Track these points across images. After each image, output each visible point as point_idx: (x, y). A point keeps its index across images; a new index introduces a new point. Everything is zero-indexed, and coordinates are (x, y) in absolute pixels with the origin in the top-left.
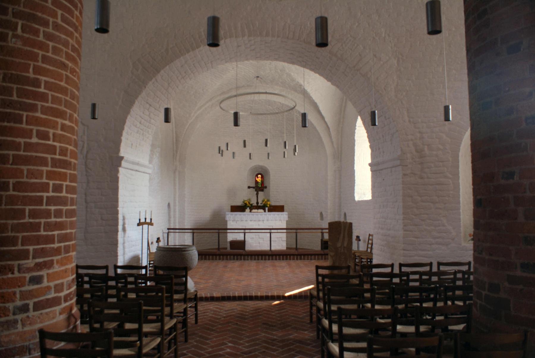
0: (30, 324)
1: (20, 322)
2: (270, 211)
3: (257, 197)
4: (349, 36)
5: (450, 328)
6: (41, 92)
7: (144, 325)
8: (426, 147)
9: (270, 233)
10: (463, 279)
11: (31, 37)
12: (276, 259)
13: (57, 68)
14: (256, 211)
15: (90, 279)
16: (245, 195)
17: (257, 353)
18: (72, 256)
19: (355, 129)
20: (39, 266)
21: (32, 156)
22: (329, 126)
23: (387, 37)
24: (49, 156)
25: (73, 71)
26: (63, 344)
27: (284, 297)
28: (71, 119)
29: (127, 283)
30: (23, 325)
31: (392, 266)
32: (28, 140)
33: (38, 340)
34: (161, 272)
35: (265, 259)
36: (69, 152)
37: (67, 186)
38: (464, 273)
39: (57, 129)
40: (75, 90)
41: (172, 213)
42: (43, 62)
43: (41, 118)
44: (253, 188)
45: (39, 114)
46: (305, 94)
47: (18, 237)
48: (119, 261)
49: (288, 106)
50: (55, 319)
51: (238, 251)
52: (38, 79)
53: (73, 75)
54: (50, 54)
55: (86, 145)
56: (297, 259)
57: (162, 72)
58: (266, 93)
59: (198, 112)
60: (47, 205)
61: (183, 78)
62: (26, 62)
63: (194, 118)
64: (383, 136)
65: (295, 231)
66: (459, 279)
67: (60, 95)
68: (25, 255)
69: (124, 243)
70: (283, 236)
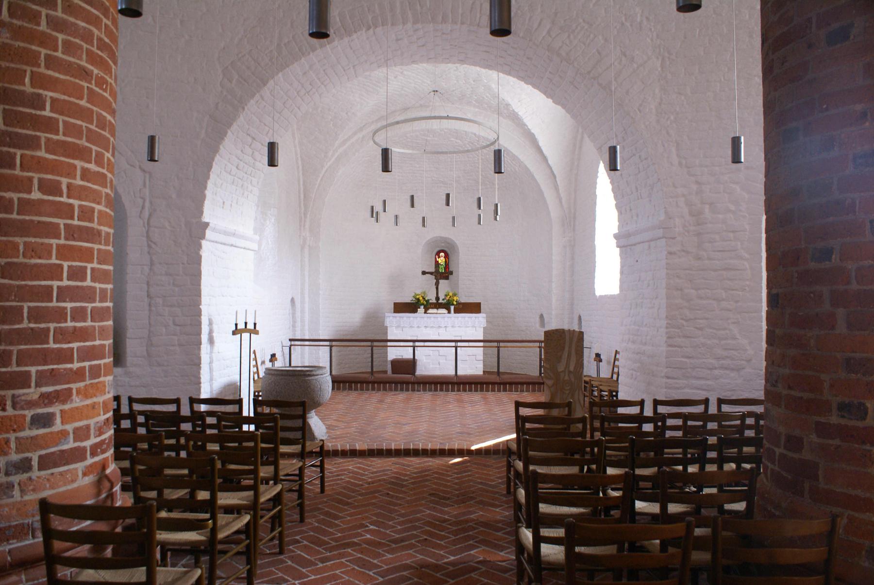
0: (34, 490)
1: (16, 486)
2: (457, 311)
3: (437, 288)
4: (581, 21)
5: (727, 507)
6: (45, 116)
7: (220, 494)
8: (707, 206)
9: (414, 347)
10: (756, 427)
11: (25, 24)
12: (465, 390)
13: (72, 76)
14: (435, 311)
15: (147, 419)
17: (413, 541)
18: (104, 382)
19: (597, 177)
20: (47, 399)
21: (32, 221)
23: (645, 22)
24: (61, 222)
25: (101, 82)
26: (89, 522)
27: (470, 452)
28: (99, 161)
29: (205, 426)
30: (23, 492)
31: (641, 403)
32: (25, 196)
33: (38, 518)
34: (267, 410)
35: (447, 390)
36: (96, 214)
37: (93, 269)
38: (757, 417)
39: (75, 178)
40: (105, 114)
41: (298, 314)
42: (47, 67)
43: (46, 159)
44: (431, 273)
45: (42, 153)
46: (515, 119)
47: (11, 352)
48: (202, 390)
49: (488, 140)
50: (76, 483)
51: (404, 377)
52: (39, 95)
53: (101, 88)
54: (59, 54)
55: (147, 204)
56: (499, 391)
57: (271, 83)
58: (448, 118)
59: (341, 150)
60: (58, 301)
61: (308, 92)
62: (18, 66)
63: (333, 159)
64: (637, 188)
65: (495, 344)
66: (750, 427)
67: (79, 122)
68: (23, 380)
69: (211, 363)
70: (478, 352)
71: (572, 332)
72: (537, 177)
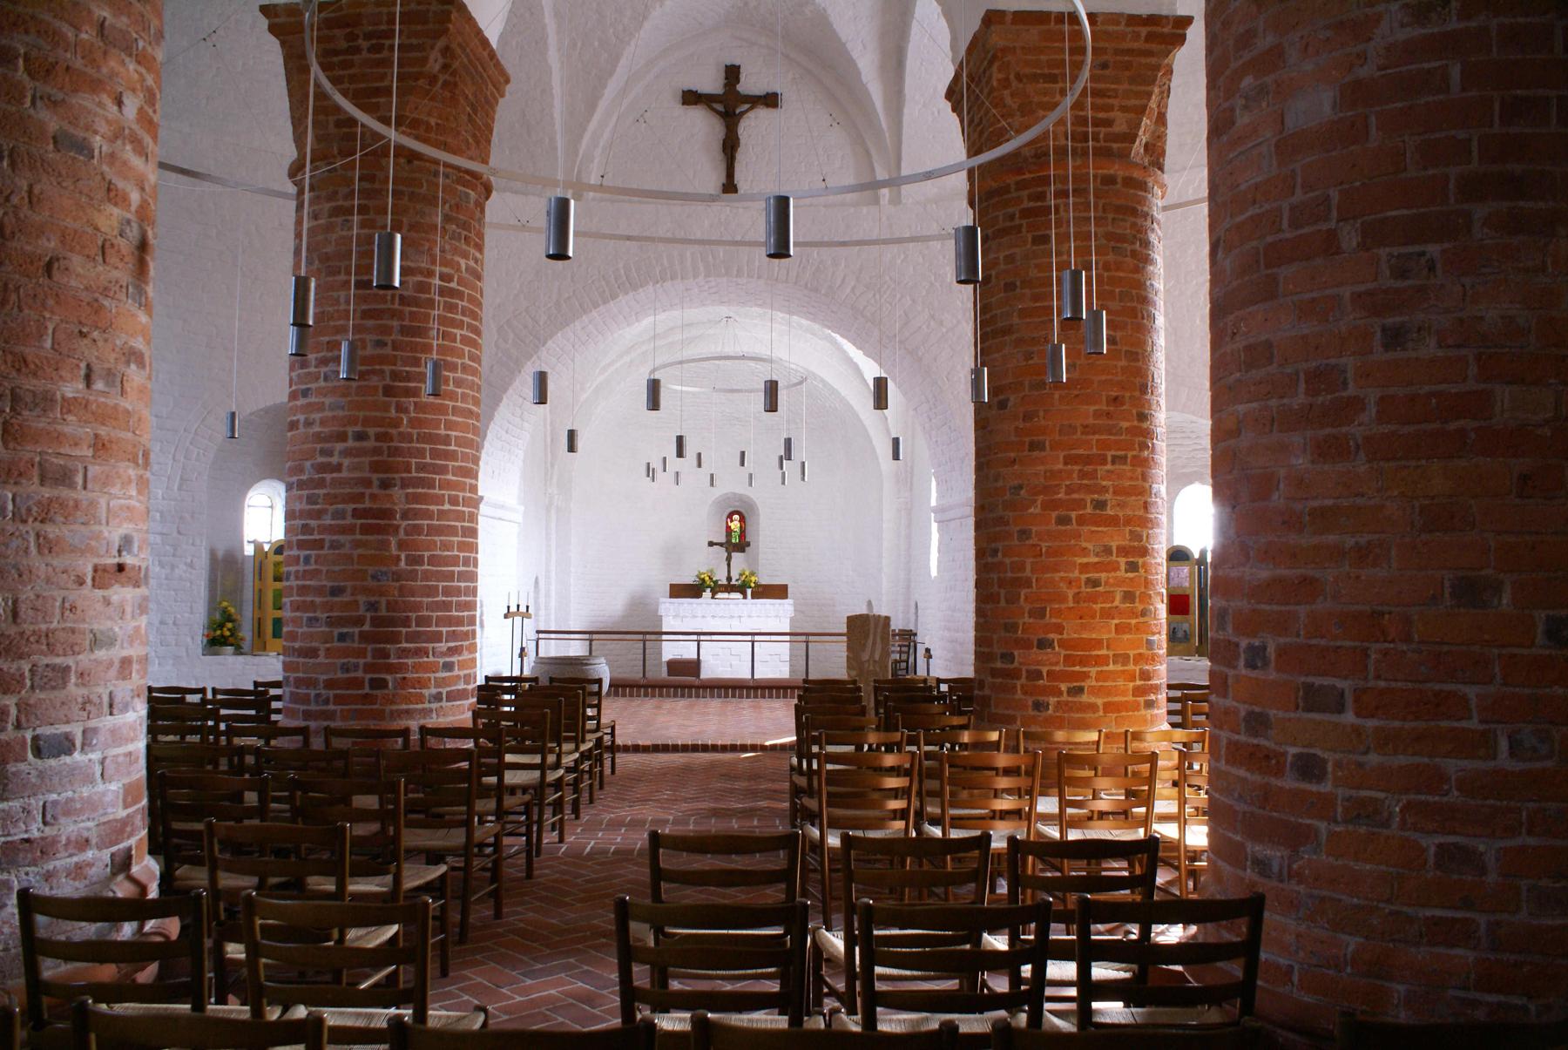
12: (763, 697)
14: (725, 595)
16: (705, 562)
27: (763, 748)
35: (741, 697)
44: (721, 545)
45: (450, 477)
51: (685, 680)
57: (550, 343)
68: (437, 637)
70: (783, 649)
72: (862, 417)
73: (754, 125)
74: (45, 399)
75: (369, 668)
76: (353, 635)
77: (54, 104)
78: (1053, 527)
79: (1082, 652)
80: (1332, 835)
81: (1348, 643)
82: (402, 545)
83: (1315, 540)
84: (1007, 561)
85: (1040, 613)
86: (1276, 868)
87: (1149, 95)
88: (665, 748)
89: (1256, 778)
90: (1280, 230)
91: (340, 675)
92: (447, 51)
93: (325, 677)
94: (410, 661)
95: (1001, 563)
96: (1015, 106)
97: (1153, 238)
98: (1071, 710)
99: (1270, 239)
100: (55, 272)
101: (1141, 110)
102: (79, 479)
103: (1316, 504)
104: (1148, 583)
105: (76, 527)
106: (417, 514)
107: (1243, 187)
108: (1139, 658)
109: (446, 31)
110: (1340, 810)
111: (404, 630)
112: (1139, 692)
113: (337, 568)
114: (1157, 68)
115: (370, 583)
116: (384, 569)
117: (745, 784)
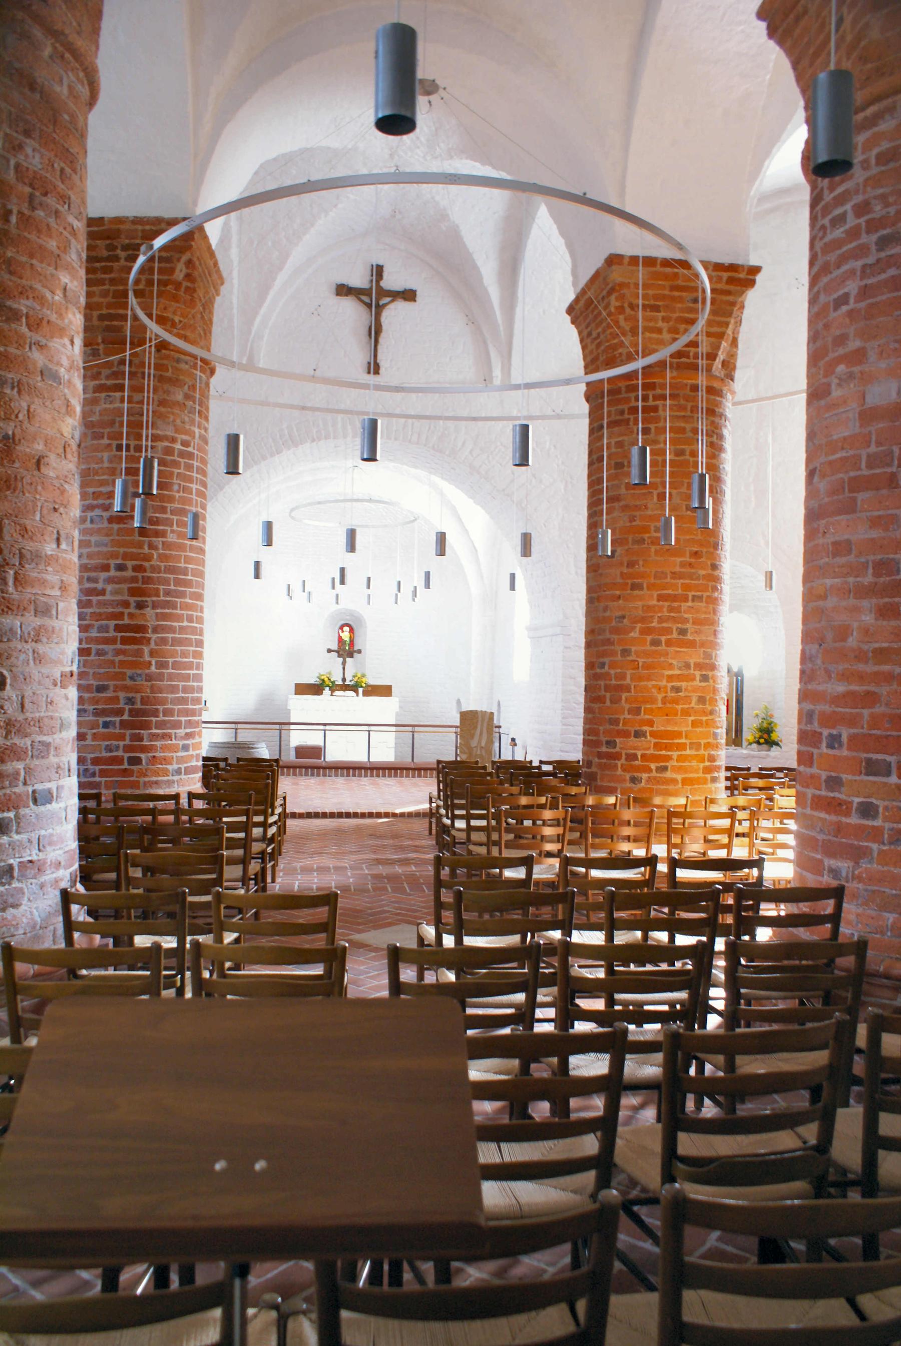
2: (366, 694)
12: (378, 776)
20: (189, 736)
22: (476, 545)
27: (394, 815)
35: (360, 776)
45: (188, 600)
51: (311, 761)
56: (413, 777)
71: (484, 713)
73: (395, 314)
74: (37, 556)
75: (127, 749)
76: (114, 723)
77: (41, 347)
78: (648, 647)
79: (667, 741)
80: (880, 852)
81: (894, 733)
82: (152, 653)
83: (876, 668)
84: (612, 672)
85: (637, 711)
86: (844, 874)
87: (727, 324)
88: (317, 815)
89: (833, 818)
90: (860, 469)
91: (105, 754)
92: (189, 263)
93: (92, 756)
94: (158, 744)
95: (608, 674)
96: (627, 328)
97: (725, 432)
98: (658, 783)
99: (852, 474)
100: (42, 467)
101: (721, 336)
102: (54, 613)
103: (877, 645)
104: (715, 691)
105: (52, 645)
106: (164, 629)
107: (835, 437)
108: (708, 746)
109: (190, 247)
110: (886, 836)
111: (154, 719)
112: (708, 770)
113: (102, 671)
114: (733, 304)
115: (129, 682)
116: (139, 672)
117: (391, 842)
